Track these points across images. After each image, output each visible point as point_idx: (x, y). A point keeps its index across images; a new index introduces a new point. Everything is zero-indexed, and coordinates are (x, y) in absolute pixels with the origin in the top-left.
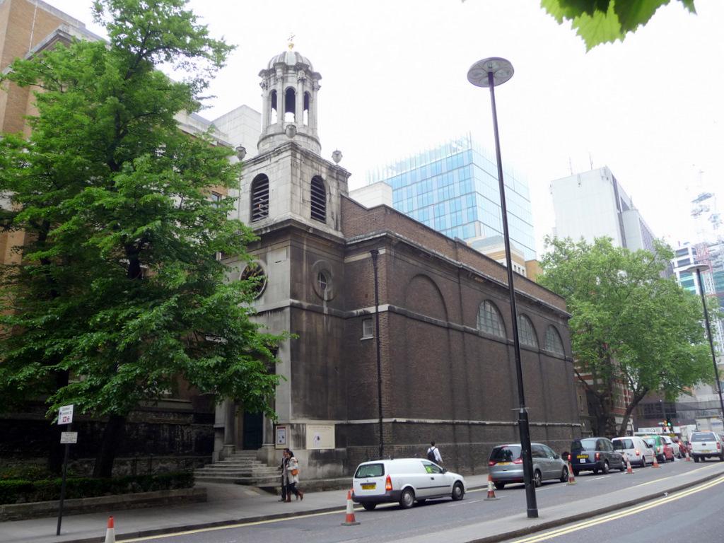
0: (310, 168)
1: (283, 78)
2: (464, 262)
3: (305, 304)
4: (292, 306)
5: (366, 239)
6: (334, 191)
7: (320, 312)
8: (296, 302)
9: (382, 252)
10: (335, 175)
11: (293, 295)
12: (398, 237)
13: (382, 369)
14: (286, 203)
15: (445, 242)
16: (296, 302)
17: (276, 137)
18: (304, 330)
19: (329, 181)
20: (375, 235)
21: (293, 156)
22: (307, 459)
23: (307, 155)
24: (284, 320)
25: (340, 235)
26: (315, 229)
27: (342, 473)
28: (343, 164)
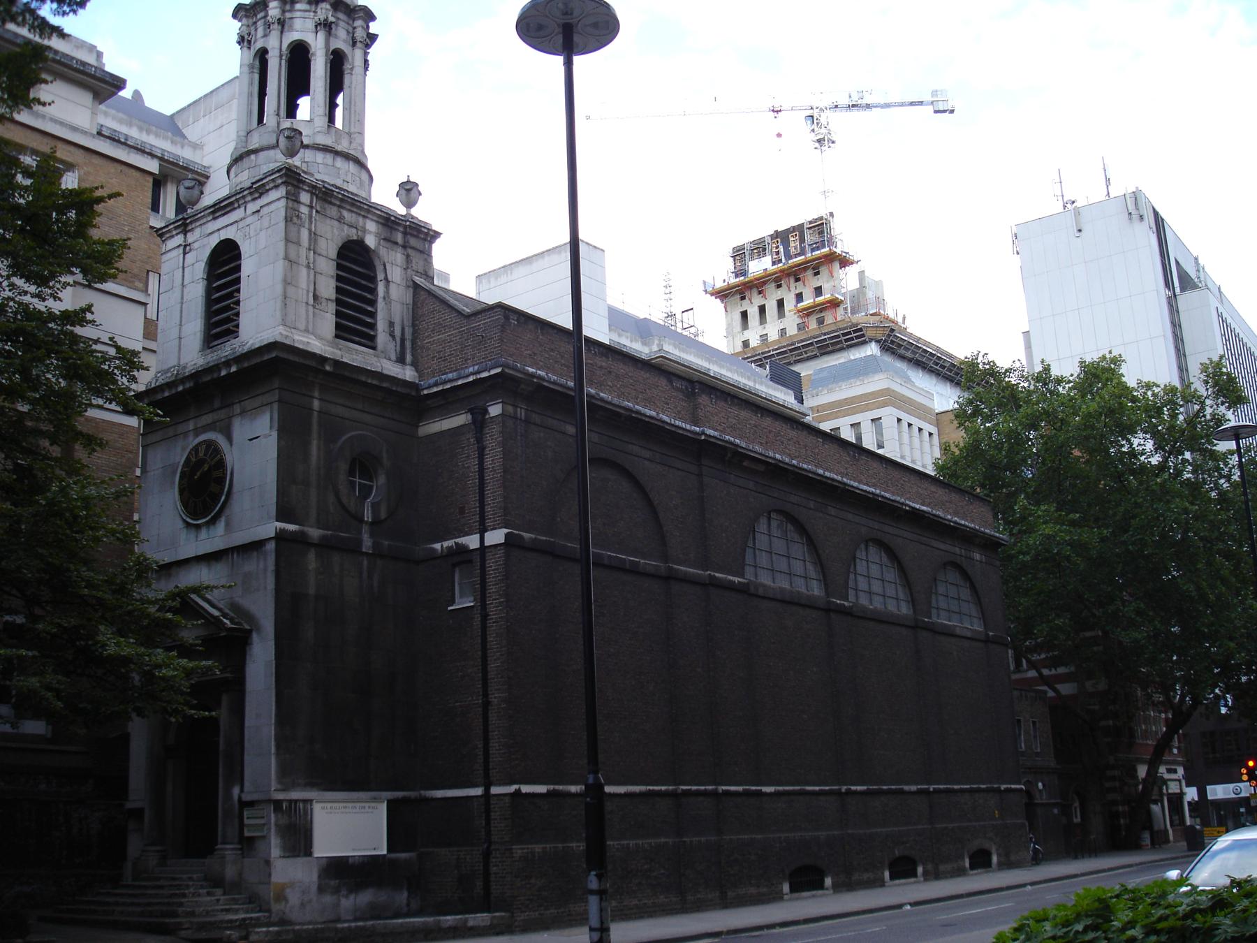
0: (336, 223)
1: (282, 23)
2: (715, 427)
3: (315, 533)
4: (280, 537)
5: (460, 382)
6: (396, 274)
7: (352, 549)
8: (292, 527)
9: (495, 410)
10: (399, 238)
11: (283, 513)
12: (532, 375)
13: (491, 675)
14: (282, 307)
15: (663, 382)
16: (292, 527)
17: (262, 155)
18: (312, 591)
19: (383, 252)
20: (479, 372)
21: (292, 198)
22: (315, 877)
23: (325, 195)
24: (264, 568)
25: (408, 374)
26: (337, 363)
27: (405, 910)
28: (420, 212)
